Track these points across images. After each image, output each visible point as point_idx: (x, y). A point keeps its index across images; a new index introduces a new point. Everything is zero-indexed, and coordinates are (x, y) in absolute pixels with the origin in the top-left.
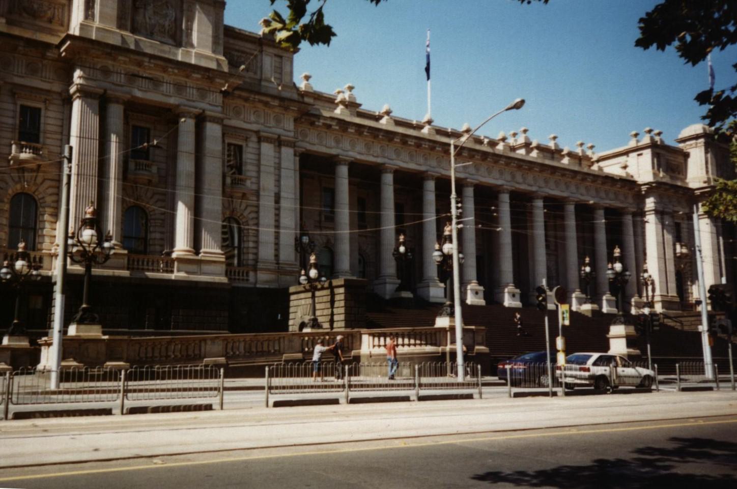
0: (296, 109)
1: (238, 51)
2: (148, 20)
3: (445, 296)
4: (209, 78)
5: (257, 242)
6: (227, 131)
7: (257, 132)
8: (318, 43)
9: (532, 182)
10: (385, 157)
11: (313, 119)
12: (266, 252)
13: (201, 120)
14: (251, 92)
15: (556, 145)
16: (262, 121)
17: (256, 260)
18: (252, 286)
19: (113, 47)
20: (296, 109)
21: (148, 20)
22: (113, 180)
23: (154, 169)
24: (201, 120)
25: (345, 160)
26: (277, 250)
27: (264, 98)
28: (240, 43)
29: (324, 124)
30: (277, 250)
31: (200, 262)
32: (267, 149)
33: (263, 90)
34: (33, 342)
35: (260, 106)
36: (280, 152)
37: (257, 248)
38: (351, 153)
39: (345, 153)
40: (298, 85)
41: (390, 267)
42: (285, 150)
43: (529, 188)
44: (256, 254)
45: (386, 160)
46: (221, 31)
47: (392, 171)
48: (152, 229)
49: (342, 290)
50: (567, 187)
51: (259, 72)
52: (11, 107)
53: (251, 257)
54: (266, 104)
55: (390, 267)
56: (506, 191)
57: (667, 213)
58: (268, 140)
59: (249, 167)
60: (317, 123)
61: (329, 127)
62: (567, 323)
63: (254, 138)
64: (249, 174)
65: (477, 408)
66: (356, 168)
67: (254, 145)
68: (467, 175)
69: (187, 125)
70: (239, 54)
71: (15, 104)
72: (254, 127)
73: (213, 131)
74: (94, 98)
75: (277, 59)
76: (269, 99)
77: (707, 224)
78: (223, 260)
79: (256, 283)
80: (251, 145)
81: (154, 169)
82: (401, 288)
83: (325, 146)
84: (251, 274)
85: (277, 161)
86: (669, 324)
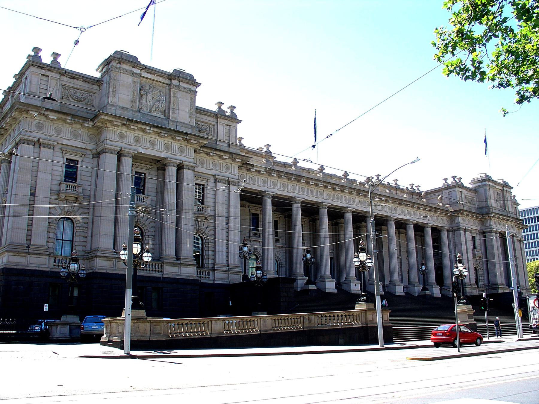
0: (240, 161)
1: (201, 122)
2: (148, 103)
3: (361, 289)
4: (186, 140)
5: (214, 251)
6: (197, 175)
7: (215, 176)
8: (140, 62)
11: (249, 167)
12: (221, 258)
13: (180, 168)
14: (211, 148)
16: (218, 169)
17: (214, 264)
18: (212, 282)
20: (240, 161)
21: (148, 103)
23: (149, 201)
24: (180, 168)
26: (228, 257)
27: (219, 153)
28: (203, 117)
29: (256, 170)
30: (228, 257)
31: (180, 264)
32: (221, 187)
33: (218, 148)
34: (81, 320)
35: (217, 158)
37: (214, 255)
38: (273, 190)
41: (299, 269)
43: (386, 214)
44: (214, 259)
45: (296, 195)
46: (194, 110)
51: (215, 136)
52: (61, 159)
53: (210, 261)
54: (221, 157)
55: (299, 269)
58: (221, 181)
59: (209, 200)
60: (251, 170)
61: (259, 172)
63: (212, 180)
64: (208, 204)
67: (213, 185)
68: (347, 205)
69: (172, 171)
70: (203, 124)
71: (63, 157)
72: (213, 172)
73: (187, 174)
74: (114, 154)
75: (228, 127)
76: (222, 154)
77: (221, 104)
78: (196, 264)
79: (214, 280)
80: (210, 184)
81: (149, 201)
82: (309, 282)
83: (256, 184)
84: (211, 273)
86: (443, 326)
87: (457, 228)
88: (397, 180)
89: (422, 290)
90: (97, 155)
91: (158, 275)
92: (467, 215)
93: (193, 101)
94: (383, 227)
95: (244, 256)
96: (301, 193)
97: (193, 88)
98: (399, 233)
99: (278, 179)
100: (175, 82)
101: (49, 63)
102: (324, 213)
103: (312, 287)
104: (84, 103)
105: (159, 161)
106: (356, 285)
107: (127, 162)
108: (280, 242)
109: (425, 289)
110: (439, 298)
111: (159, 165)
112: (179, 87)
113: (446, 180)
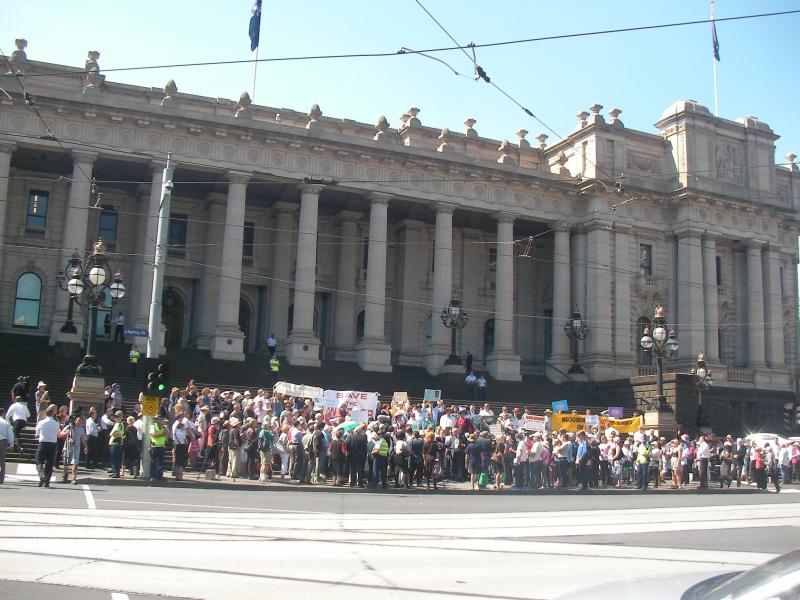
9: (453, 192)
10: (559, 213)
15: (617, 121)
19: (705, 178)
22: (696, 295)
25: (239, 177)
36: (614, 240)
39: (508, 209)
40: (532, 146)
42: (621, 239)
45: (503, 207)
47: (385, 201)
48: (725, 344)
49: (673, 385)
50: (750, 224)
56: (506, 219)
57: (624, 231)
60: (243, 137)
62: (755, 484)
65: (192, 318)
66: (522, 227)
85: (612, 248)
87: (592, 223)
88: (415, 111)
89: (447, 362)
90: (675, 239)
91: (750, 386)
92: (758, 212)
93: (772, 157)
94: (344, 212)
95: (452, 323)
96: (240, 161)
97: (769, 142)
98: (463, 236)
99: (378, 164)
100: (751, 137)
101: (776, 163)
102: (380, 213)
103: (579, 378)
104: (650, 171)
105: (737, 241)
106: (306, 348)
107: (711, 244)
108: (254, 265)
109: (576, 369)
110: (388, 374)
111: (736, 246)
112: (756, 142)
113: (585, 115)
